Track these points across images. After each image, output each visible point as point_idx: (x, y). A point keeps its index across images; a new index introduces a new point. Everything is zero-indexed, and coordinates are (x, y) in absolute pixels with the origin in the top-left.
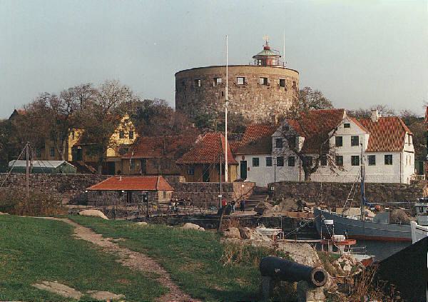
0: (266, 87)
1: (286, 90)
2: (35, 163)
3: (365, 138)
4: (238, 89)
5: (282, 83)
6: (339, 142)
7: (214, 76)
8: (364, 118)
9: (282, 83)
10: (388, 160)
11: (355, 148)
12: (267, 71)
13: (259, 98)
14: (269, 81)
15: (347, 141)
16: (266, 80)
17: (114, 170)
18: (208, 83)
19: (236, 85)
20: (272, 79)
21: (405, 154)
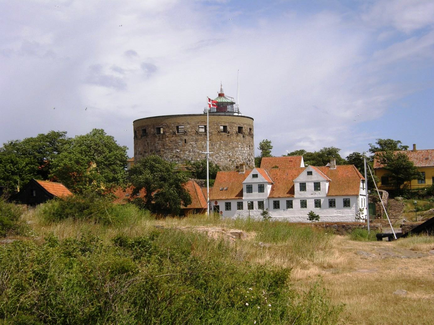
0: (227, 134)
1: (244, 137)
2: (208, 192)
3: (325, 186)
4: (199, 137)
5: (240, 129)
6: (303, 187)
7: (177, 125)
8: (318, 224)
9: (240, 129)
10: (347, 204)
11: (317, 192)
12: (224, 120)
13: (220, 146)
14: (228, 129)
15: (310, 186)
16: (225, 127)
17: (326, 165)
18: (171, 131)
19: (197, 133)
20: (231, 127)
21: (360, 197)
